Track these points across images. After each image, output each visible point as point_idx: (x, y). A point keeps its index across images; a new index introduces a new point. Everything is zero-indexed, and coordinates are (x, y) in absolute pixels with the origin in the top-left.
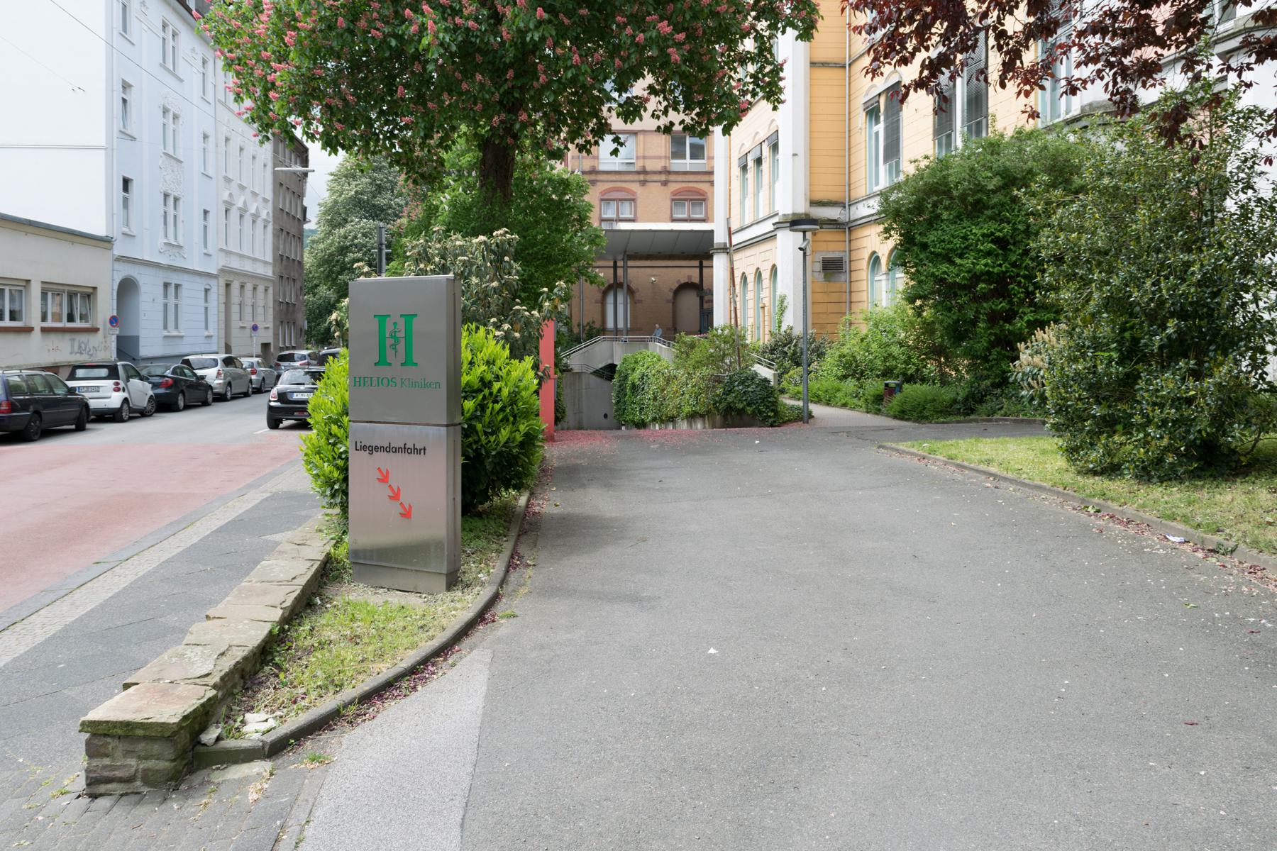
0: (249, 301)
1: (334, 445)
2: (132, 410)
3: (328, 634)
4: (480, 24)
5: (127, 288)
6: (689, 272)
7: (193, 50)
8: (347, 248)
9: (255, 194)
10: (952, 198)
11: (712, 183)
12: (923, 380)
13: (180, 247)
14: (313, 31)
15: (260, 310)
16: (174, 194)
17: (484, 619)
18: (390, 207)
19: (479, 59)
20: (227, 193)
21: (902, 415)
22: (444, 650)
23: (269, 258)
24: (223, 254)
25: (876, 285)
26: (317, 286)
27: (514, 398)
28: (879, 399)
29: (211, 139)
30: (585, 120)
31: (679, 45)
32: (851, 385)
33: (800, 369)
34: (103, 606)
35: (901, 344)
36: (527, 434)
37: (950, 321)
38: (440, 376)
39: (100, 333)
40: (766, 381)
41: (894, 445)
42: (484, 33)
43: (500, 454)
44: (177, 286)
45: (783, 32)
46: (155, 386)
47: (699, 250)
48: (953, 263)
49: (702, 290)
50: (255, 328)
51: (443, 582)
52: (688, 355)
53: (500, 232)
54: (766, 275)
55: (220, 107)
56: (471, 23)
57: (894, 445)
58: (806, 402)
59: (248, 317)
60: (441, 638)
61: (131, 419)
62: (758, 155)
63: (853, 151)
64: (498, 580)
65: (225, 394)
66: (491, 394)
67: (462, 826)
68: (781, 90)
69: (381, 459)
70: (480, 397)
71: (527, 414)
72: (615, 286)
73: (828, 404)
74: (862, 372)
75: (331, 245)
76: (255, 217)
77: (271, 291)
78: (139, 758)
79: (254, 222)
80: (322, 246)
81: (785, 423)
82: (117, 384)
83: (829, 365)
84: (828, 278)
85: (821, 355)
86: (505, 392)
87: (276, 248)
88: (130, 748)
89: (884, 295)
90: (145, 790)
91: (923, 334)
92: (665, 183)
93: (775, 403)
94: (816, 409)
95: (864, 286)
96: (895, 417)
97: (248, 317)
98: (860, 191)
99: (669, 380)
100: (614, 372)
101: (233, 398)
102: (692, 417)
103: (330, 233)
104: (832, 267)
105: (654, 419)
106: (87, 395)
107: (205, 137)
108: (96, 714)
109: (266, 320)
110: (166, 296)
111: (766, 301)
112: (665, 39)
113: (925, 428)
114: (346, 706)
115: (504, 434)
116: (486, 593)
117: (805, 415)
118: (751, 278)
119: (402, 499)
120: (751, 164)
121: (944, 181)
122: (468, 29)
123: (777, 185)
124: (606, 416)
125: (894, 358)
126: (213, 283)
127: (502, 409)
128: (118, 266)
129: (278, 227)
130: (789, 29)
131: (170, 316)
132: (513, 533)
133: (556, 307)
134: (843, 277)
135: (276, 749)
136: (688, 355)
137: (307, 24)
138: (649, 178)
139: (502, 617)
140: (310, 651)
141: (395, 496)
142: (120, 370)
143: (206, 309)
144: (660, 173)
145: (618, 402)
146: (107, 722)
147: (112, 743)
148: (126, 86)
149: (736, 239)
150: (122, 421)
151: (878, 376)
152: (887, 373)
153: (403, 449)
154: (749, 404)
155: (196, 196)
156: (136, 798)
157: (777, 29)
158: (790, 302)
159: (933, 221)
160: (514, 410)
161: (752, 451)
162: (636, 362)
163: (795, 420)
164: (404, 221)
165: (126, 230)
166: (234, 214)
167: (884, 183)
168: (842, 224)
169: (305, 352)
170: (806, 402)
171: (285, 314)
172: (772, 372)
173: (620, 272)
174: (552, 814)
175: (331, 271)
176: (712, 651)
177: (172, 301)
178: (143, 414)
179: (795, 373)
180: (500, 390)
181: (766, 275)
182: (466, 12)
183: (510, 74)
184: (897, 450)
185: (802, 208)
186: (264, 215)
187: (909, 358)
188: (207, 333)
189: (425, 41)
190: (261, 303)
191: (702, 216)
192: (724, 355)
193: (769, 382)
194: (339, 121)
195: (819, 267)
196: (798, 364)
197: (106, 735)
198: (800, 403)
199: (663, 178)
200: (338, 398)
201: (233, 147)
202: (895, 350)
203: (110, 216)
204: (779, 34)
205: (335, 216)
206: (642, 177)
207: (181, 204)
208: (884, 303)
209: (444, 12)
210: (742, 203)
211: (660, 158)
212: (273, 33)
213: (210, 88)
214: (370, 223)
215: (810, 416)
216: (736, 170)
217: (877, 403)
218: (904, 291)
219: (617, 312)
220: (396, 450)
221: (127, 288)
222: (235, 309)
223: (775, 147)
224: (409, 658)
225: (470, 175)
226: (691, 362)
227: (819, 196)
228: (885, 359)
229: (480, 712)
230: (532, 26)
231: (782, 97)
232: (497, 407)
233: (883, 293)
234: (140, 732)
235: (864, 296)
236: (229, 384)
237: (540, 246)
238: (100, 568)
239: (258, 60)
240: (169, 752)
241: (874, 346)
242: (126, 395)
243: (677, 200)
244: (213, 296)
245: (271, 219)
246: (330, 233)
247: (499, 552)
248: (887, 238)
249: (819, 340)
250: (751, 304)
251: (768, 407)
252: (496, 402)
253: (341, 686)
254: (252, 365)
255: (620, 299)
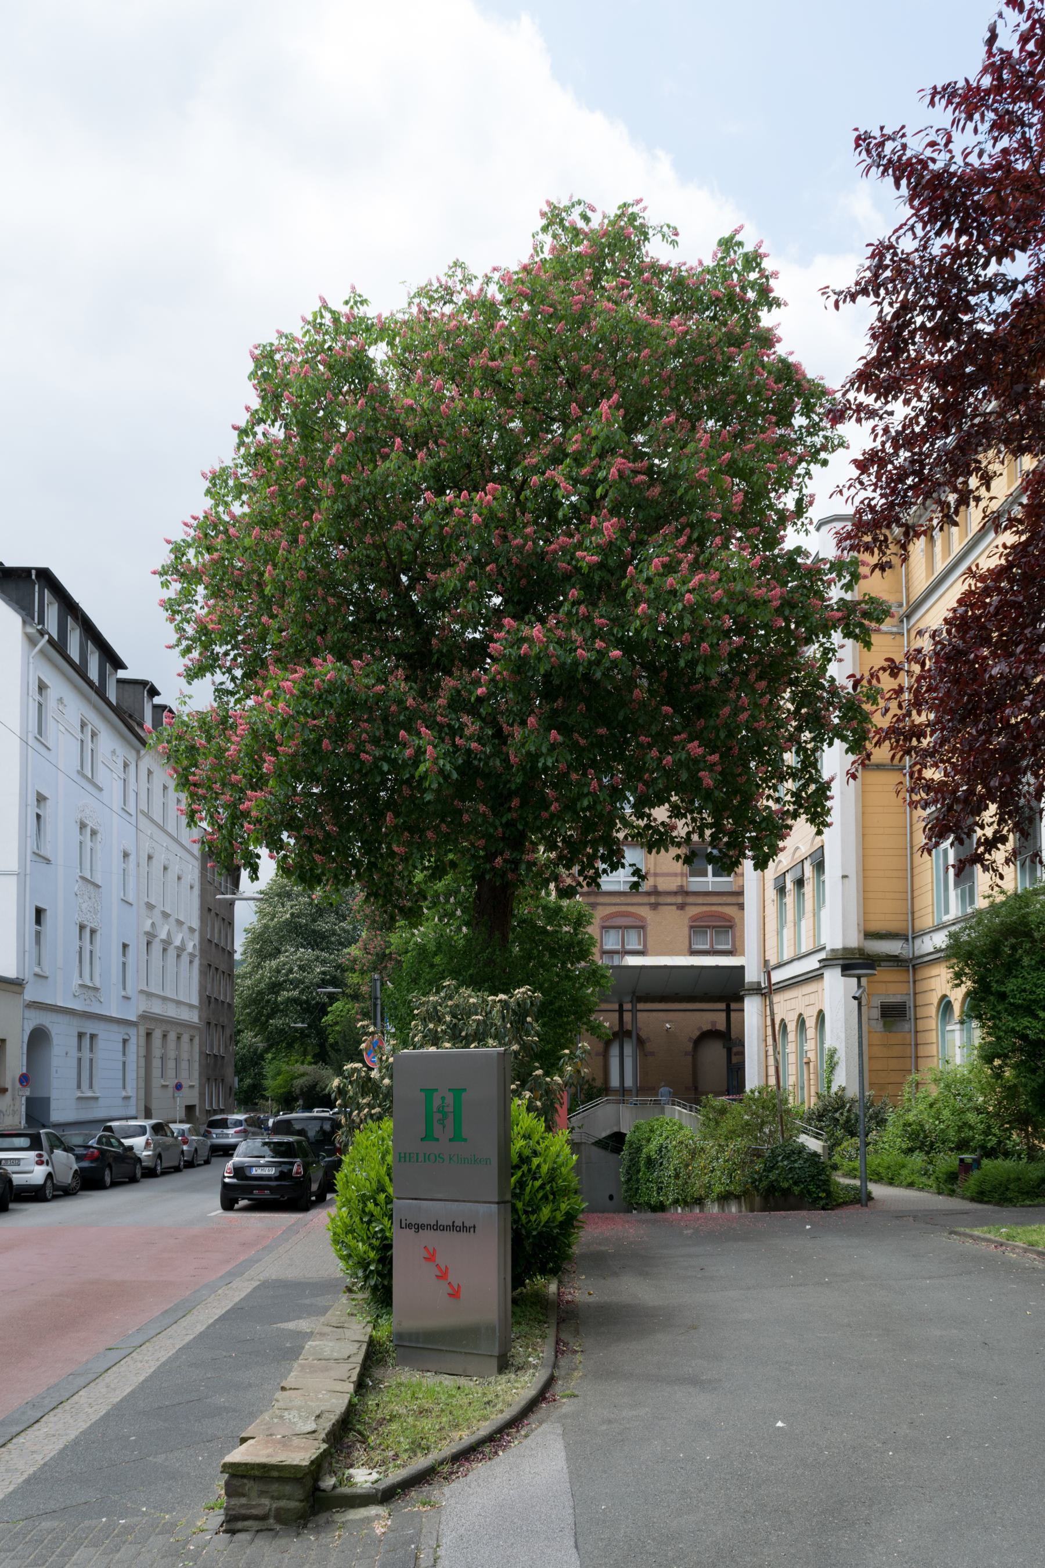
0: (172, 1054)
1: (369, 1222)
2: (55, 1188)
3: (397, 1408)
4: (484, 745)
5: (38, 1039)
6: (713, 1018)
7: (114, 752)
8: (280, 984)
9: (180, 923)
10: (1033, 941)
11: (741, 906)
12: (1007, 1154)
13: (96, 989)
14: (294, 755)
15: (184, 1065)
16: (90, 925)
17: (544, 1399)
18: (334, 934)
19: (480, 783)
20: (149, 922)
21: (980, 1197)
22: (516, 1422)
23: (195, 1001)
24: (143, 997)
25: (948, 1036)
26: (240, 1031)
27: (553, 1175)
28: (952, 1177)
29: (132, 858)
30: (595, 844)
31: (711, 767)
32: (919, 1160)
33: (856, 1140)
34: (143, 1386)
35: (979, 1110)
36: (567, 1213)
37: (1034, 1085)
38: (490, 1151)
39: (9, 1094)
40: (815, 1154)
41: (968, 1231)
42: (489, 757)
43: (540, 1234)
44: (93, 1037)
45: (830, 744)
46: (79, 1158)
47: (728, 990)
48: (1036, 1017)
49: (731, 1041)
50: (179, 1087)
51: (494, 1364)
52: (717, 1123)
53: (522, 990)
54: (811, 1023)
55: (142, 820)
56: (474, 745)
57: (968, 1231)
58: (865, 1180)
59: (171, 1073)
60: (508, 1415)
61: (55, 1197)
62: (799, 875)
63: (916, 871)
64: (551, 1363)
65: (155, 1169)
66: (529, 1170)
67: (576, 1547)
68: (828, 812)
69: (428, 1237)
70: (520, 1173)
71: (565, 1192)
72: (622, 1034)
73: (891, 1183)
74: (932, 1144)
75: (260, 981)
76: (181, 949)
77: (197, 1040)
78: (273, 1498)
79: (165, 950)
80: (248, 982)
81: (839, 1205)
82: (40, 1156)
83: (890, 1139)
84: (888, 1027)
85: (881, 1122)
86: (545, 1168)
87: (202, 988)
88: (264, 1488)
89: (958, 1051)
90: (278, 1527)
91: (1004, 1098)
92: (681, 907)
93: (827, 1182)
94: (877, 1190)
95: (933, 1037)
96: (972, 1200)
97: (171, 1073)
98: (926, 920)
99: (694, 1153)
100: (623, 1142)
101: (164, 1173)
102: (724, 1198)
103: (259, 966)
104: (894, 1014)
105: (676, 1202)
106: (10, 1169)
107: (126, 855)
108: (239, 1455)
109: (191, 1077)
110: (80, 1049)
111: (811, 1055)
112: (696, 761)
113: (1006, 1212)
114: (441, 1463)
115: (546, 1212)
116: (541, 1376)
117: (864, 1197)
118: (791, 1027)
119: (451, 1278)
120: (789, 885)
121: (1024, 921)
122: (469, 751)
123: (825, 913)
124: (611, 1197)
125: (971, 1128)
126: (132, 1031)
127: (542, 1187)
128: (29, 1013)
129: (206, 963)
130: (837, 741)
131: (86, 1073)
132: (553, 1321)
133: (579, 1071)
134: (907, 1027)
135: (386, 1496)
136: (717, 1123)
137: (287, 749)
138: (662, 899)
139: (563, 1397)
140: (381, 1422)
141: (443, 1276)
142: (43, 1138)
143: (124, 1063)
144: (675, 893)
145: (629, 1180)
146: (246, 1464)
147: (249, 1484)
148: (41, 799)
149: (777, 976)
150: (45, 1200)
151: (951, 1149)
152: (962, 1145)
153: (452, 1227)
154: (796, 1183)
155: (118, 925)
156: (270, 1533)
157: (822, 741)
158: (841, 1056)
159: (1012, 967)
160: (553, 1189)
161: (801, 1235)
162: (652, 1131)
163: (852, 1202)
164: (354, 950)
165: (37, 970)
166: (157, 947)
167: (955, 911)
168: (906, 961)
169: (241, 1117)
170: (865, 1180)
171: (212, 1069)
172: (821, 1143)
173: (627, 1017)
174: (654, 1539)
175: (260, 1013)
176: (780, 1424)
177: (86, 1054)
178: (65, 1192)
179: (849, 1144)
180: (539, 1166)
181: (811, 1023)
182: (467, 732)
183: (515, 802)
184: (971, 1236)
185: (854, 941)
186: (190, 948)
187: (989, 1127)
188: (124, 1094)
189: (422, 768)
190: (185, 1056)
191: (729, 947)
192: (763, 1123)
193: (819, 1156)
194: (318, 852)
195: (876, 1013)
196: (853, 1134)
197: (243, 1477)
198: (857, 1183)
199: (679, 900)
200: (373, 1174)
201: (172, 875)
202: (972, 1118)
203: (22, 953)
204: (825, 746)
205: (265, 945)
206: (652, 899)
207: (98, 936)
208: (958, 1060)
209: (440, 732)
210: (780, 933)
211: (675, 875)
212: (247, 755)
213: (132, 797)
214: (309, 954)
215: (870, 1197)
216: (771, 893)
217: (950, 1183)
218: (981, 1047)
219: (623, 1068)
220: (444, 1228)
221: (38, 1039)
222: (156, 1063)
223: (819, 866)
224: (484, 1429)
225: (447, 901)
226: (723, 1130)
227: (876, 926)
228: (960, 1129)
229: (565, 1470)
230: (544, 750)
231: (829, 819)
232: (537, 1184)
233: (955, 1047)
234: (275, 1474)
235: (933, 1050)
236: (160, 1156)
237: (555, 1001)
238: (114, 1356)
239: (224, 785)
240: (299, 1492)
241: (946, 1113)
242: (49, 1169)
243: (697, 927)
244: (132, 1047)
245: (197, 953)
246: (259, 966)
247: (544, 1337)
248: (958, 986)
249: (878, 1104)
250: (792, 1058)
251: (818, 1187)
252: (535, 1179)
253: (428, 1449)
254: (182, 1133)
255: (628, 1050)
